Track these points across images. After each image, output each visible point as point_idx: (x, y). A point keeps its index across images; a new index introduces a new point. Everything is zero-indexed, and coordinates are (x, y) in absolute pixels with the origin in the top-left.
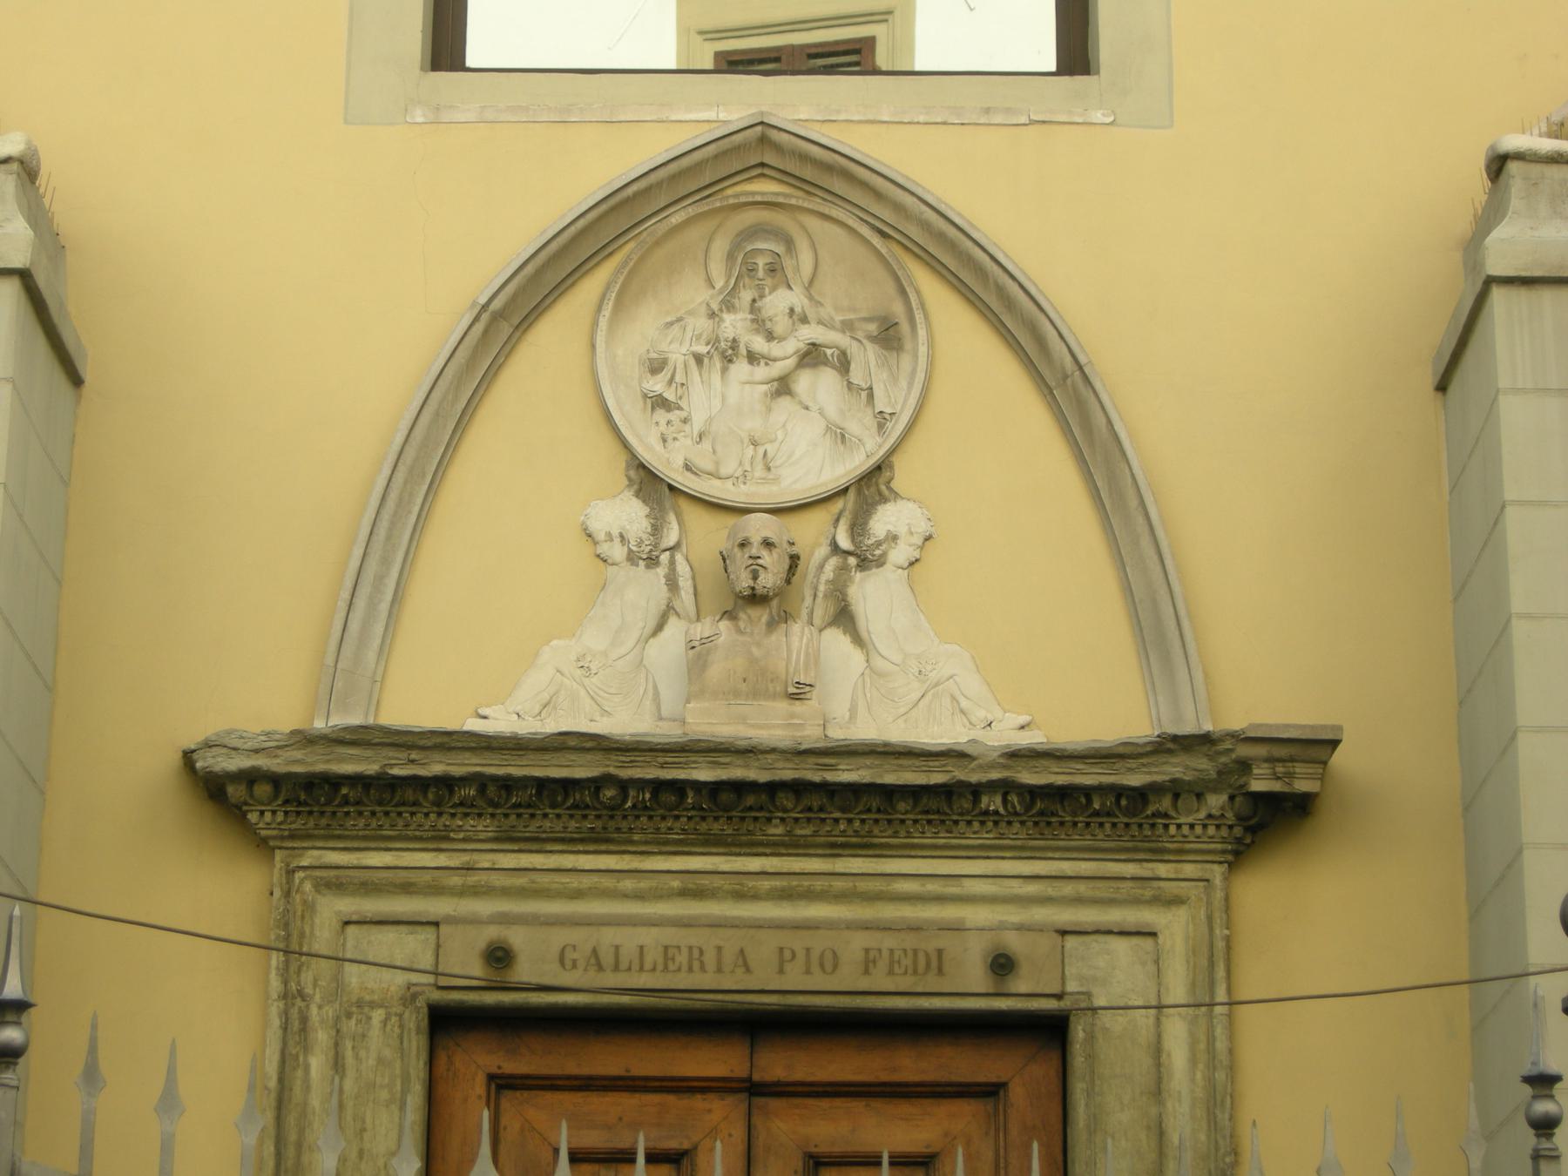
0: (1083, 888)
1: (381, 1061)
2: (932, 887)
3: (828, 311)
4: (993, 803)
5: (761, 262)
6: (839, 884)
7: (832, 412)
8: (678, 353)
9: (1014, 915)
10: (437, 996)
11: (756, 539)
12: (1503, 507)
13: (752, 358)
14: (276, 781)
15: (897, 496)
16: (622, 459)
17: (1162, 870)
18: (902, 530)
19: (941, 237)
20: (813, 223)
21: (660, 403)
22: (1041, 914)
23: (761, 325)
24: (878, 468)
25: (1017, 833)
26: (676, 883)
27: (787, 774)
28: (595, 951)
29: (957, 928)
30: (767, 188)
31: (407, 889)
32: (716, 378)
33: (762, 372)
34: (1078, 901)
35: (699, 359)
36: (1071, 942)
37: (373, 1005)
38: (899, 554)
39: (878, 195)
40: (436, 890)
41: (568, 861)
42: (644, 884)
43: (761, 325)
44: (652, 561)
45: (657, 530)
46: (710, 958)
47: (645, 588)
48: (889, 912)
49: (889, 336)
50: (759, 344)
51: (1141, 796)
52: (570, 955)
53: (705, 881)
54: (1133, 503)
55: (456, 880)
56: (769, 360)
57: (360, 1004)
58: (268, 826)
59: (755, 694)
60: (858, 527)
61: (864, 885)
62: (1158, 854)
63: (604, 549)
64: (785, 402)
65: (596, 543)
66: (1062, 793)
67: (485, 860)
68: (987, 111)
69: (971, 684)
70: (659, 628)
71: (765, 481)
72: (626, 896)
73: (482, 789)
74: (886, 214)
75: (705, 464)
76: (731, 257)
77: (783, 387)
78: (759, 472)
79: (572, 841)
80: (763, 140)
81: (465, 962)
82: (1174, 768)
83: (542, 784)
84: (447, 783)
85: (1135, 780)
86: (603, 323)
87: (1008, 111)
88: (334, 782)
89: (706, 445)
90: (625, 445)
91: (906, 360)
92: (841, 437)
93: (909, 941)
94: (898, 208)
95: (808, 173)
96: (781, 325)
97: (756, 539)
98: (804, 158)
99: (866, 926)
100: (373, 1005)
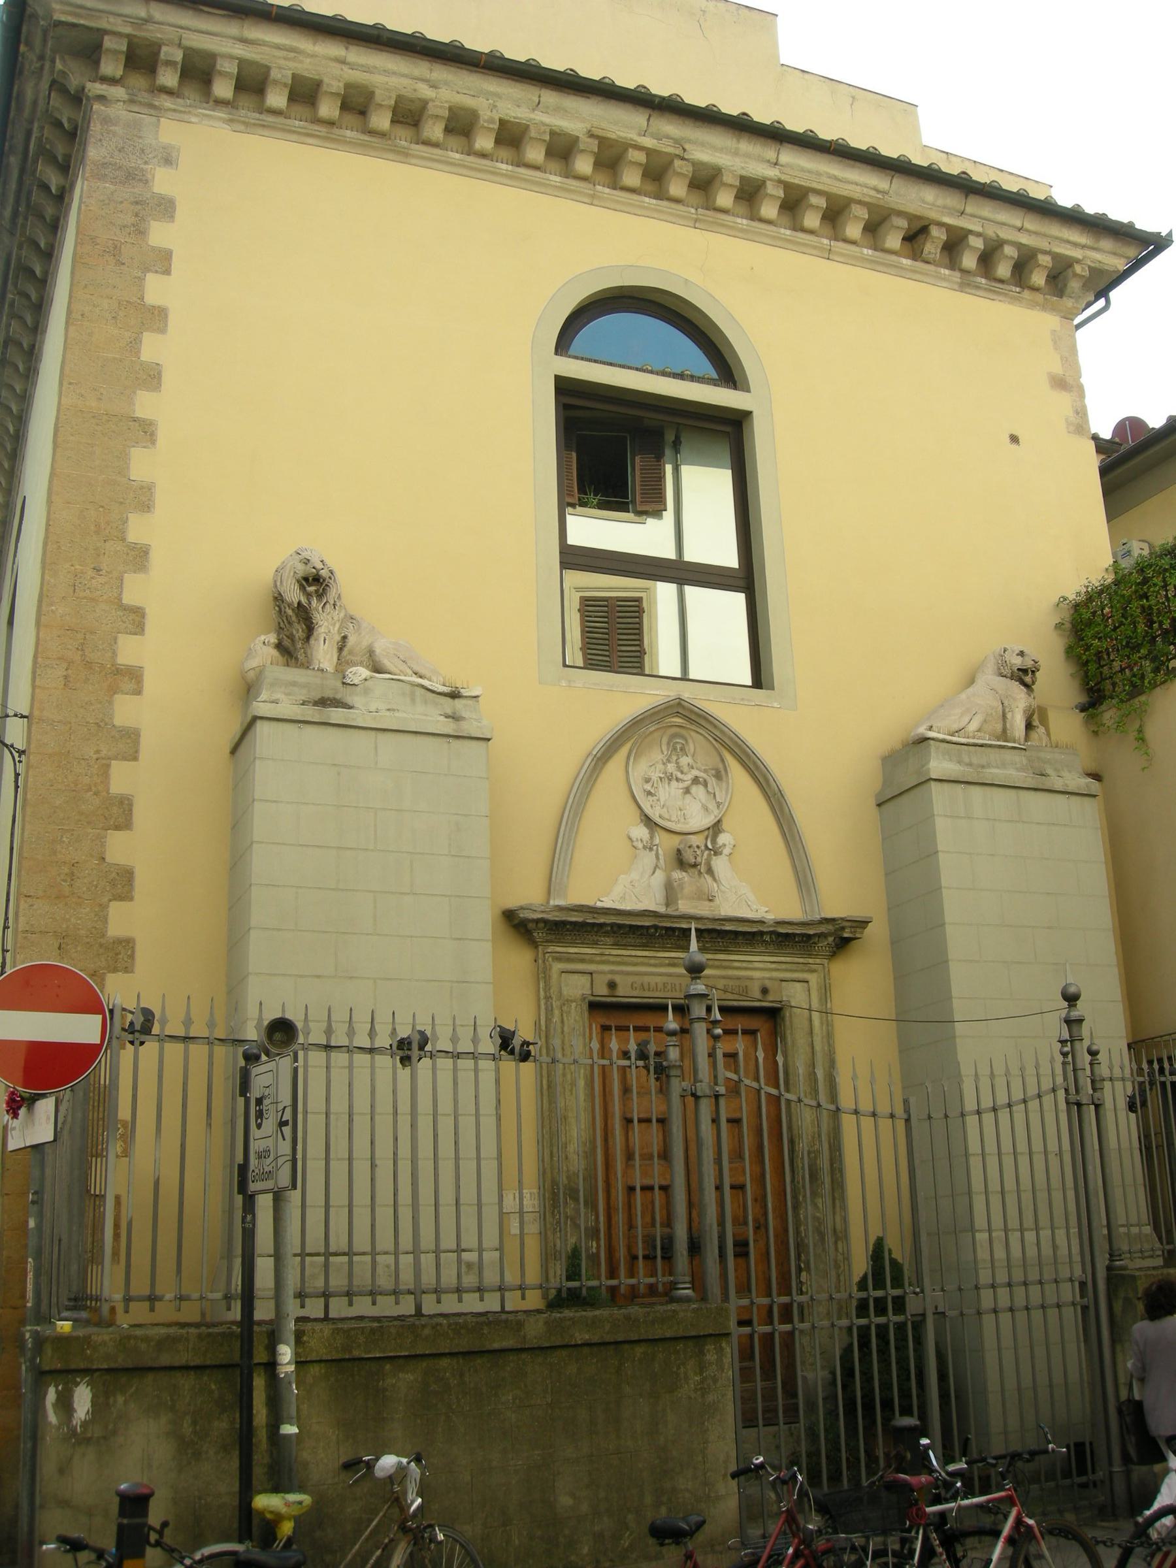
0: (788, 966)
1: (575, 1020)
2: (744, 965)
3: (699, 765)
4: (767, 938)
5: (678, 747)
6: (717, 963)
7: (703, 801)
8: (655, 776)
9: (767, 974)
10: (592, 998)
11: (695, 845)
12: (252, 843)
13: (677, 780)
14: (545, 921)
15: (724, 831)
16: (638, 812)
17: (811, 961)
18: (727, 843)
19: (736, 743)
20: (693, 734)
21: (649, 793)
22: (775, 974)
23: (679, 769)
24: (719, 821)
25: (771, 948)
26: (667, 961)
27: (710, 926)
28: (642, 985)
29: (751, 979)
30: (678, 720)
31: (582, 961)
32: (667, 786)
33: (681, 785)
34: (786, 970)
35: (661, 778)
36: (784, 984)
37: (572, 1001)
38: (726, 851)
39: (715, 726)
40: (592, 962)
41: (634, 953)
42: (657, 962)
43: (679, 769)
44: (651, 849)
45: (652, 838)
46: (678, 988)
47: (648, 859)
48: (730, 973)
49: (718, 776)
50: (679, 775)
51: (809, 937)
52: (635, 985)
53: (676, 961)
54: (798, 838)
55: (598, 958)
56: (683, 781)
57: (567, 1000)
58: (540, 938)
59: (699, 898)
60: (714, 841)
61: (724, 964)
62: (810, 956)
63: (635, 844)
64: (688, 795)
65: (632, 841)
66: (787, 936)
67: (607, 952)
68: (743, 699)
69: (752, 897)
70: (654, 873)
71: (684, 823)
72: (651, 965)
73: (612, 927)
74: (718, 733)
75: (666, 816)
76: (668, 744)
77: (687, 791)
78: (682, 820)
79: (636, 946)
80: (679, 704)
81: (602, 990)
82: (823, 929)
83: (631, 926)
84: (602, 925)
85: (811, 932)
86: (631, 763)
87: (748, 700)
88: (564, 923)
89: (665, 810)
90: (640, 807)
91: (724, 785)
92: (706, 809)
93: (737, 983)
94: (722, 732)
95: (693, 717)
96: (686, 769)
97: (695, 845)
98: (692, 711)
99: (724, 977)
100: (572, 1001)
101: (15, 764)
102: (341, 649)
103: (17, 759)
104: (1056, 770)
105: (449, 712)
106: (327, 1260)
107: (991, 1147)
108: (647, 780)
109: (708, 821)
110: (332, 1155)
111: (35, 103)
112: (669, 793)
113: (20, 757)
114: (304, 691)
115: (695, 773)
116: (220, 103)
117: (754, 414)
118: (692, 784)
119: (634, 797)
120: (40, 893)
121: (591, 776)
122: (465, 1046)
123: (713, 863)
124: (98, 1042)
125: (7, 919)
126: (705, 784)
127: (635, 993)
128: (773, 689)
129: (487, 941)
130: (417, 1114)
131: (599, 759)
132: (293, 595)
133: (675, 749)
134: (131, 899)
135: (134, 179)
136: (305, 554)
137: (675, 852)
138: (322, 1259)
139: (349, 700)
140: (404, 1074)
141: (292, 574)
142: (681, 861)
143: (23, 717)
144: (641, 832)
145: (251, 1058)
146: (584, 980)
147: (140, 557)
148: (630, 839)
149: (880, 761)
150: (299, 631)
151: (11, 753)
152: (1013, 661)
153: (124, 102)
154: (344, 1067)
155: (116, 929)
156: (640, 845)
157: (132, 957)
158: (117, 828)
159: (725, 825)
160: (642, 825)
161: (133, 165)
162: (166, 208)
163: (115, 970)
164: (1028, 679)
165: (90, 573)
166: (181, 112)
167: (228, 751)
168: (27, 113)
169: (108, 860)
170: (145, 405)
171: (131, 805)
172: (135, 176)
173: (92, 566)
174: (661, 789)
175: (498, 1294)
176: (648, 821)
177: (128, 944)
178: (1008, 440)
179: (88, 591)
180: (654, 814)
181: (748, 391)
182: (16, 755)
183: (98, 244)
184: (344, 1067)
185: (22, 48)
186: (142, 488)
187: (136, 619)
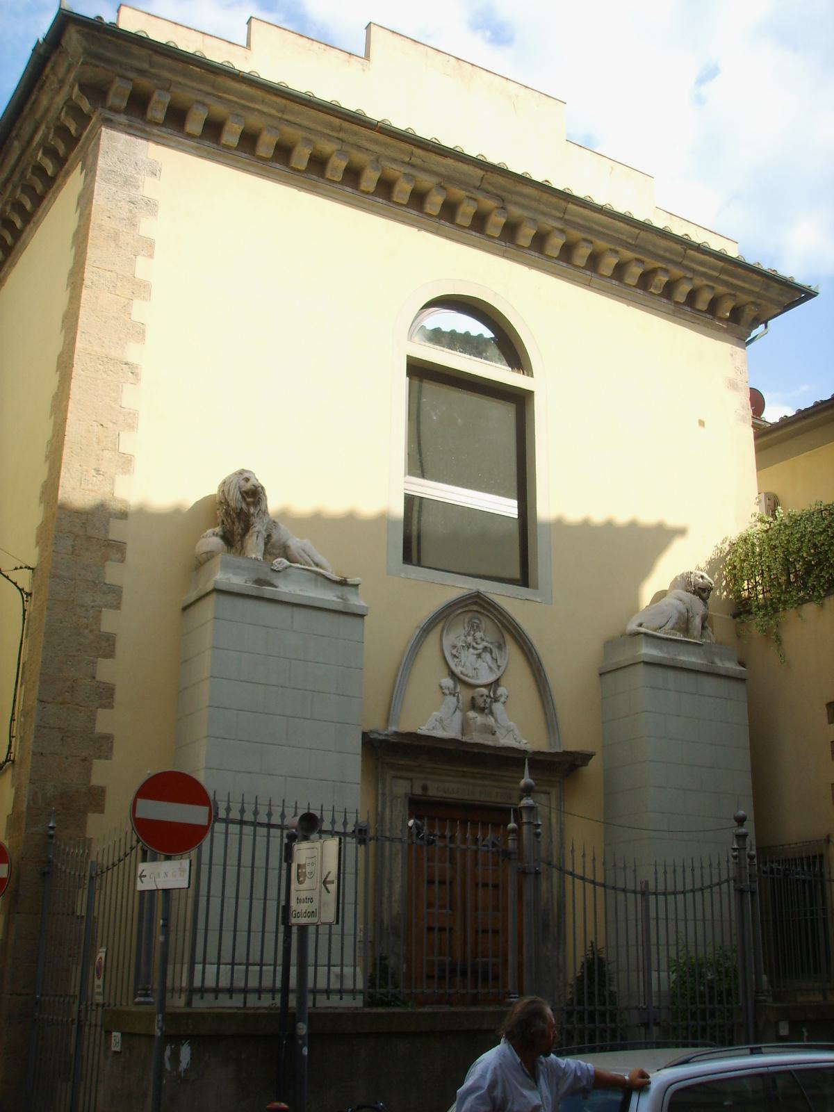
3: (488, 639)
13: (474, 648)
21: (455, 656)
30: (475, 608)
33: (476, 652)
37: (399, 797)
38: (503, 699)
43: (475, 639)
44: (454, 695)
45: (455, 687)
50: (475, 646)
60: (495, 693)
64: (479, 659)
70: (455, 712)
75: (465, 672)
76: (469, 622)
77: (479, 656)
81: (418, 791)
96: (479, 641)
101: (24, 603)
102: (266, 544)
103: (25, 599)
106: (247, 968)
108: (454, 647)
109: (492, 678)
110: (254, 896)
111: (47, 110)
112: (468, 657)
113: (27, 597)
115: (485, 644)
116: (190, 136)
117: (535, 393)
118: (483, 651)
119: (444, 658)
121: (418, 643)
122: (263, 818)
123: (493, 707)
124: (207, 824)
125: (13, 714)
126: (491, 652)
129: (358, 754)
130: (287, 870)
131: (425, 630)
134: (112, 707)
135: (130, 184)
136: (246, 475)
137: (470, 698)
138: (244, 967)
139: (276, 582)
140: (362, 848)
141: (237, 489)
142: (473, 705)
143: (29, 568)
144: (448, 682)
145: (292, 838)
146: (407, 784)
148: (441, 687)
150: (238, 528)
151: (22, 596)
153: (125, 125)
154: (264, 836)
155: (101, 728)
156: (447, 692)
157: (111, 748)
158: (105, 656)
159: (503, 682)
161: (129, 174)
162: (151, 206)
163: (99, 757)
164: (704, 595)
165: (93, 472)
166: (164, 138)
167: (181, 607)
168: (38, 116)
169: (98, 678)
170: (133, 353)
171: (114, 641)
172: (128, 182)
174: (462, 655)
176: (452, 674)
177: (108, 738)
178: (698, 423)
179: (90, 486)
180: (457, 670)
181: (532, 376)
182: (25, 596)
183: (103, 231)
184: (264, 836)
185: (48, 70)
186: (130, 413)
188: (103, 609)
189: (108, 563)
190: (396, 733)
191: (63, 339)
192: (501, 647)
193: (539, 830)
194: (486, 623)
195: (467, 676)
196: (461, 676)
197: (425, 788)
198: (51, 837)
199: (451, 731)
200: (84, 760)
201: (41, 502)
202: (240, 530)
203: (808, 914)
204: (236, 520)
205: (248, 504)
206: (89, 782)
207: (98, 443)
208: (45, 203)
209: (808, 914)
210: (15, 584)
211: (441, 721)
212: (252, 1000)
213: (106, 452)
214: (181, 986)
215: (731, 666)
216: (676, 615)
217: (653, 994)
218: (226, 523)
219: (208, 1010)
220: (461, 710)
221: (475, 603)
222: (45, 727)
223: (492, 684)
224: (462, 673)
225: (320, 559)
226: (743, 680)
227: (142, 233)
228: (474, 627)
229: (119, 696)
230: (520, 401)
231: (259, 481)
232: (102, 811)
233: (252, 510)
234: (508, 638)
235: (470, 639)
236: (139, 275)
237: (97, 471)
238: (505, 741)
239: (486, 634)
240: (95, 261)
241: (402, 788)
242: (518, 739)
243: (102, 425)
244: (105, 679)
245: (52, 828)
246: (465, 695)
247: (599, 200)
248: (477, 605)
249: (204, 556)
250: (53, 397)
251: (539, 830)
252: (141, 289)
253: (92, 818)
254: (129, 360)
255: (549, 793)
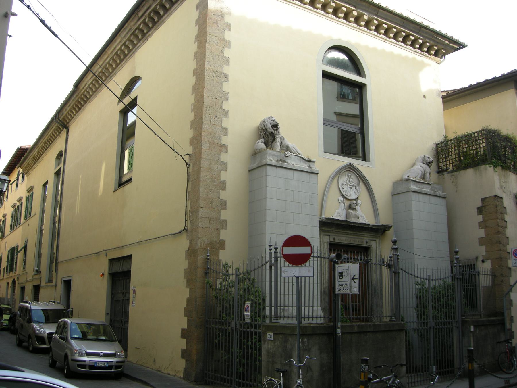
13: (349, 185)
33: (350, 187)
38: (359, 205)
45: (343, 200)
50: (350, 184)
75: (347, 194)
81: (332, 240)
96: (351, 182)
104: (437, 190)
105: (308, 165)
107: (286, 293)
108: (343, 185)
114: (277, 157)
117: (367, 85)
120: (204, 207)
124: (310, 253)
126: (355, 187)
127: (339, 241)
128: (370, 162)
132: (270, 129)
133: (349, 177)
144: (341, 198)
146: (328, 237)
147: (226, 113)
148: (339, 200)
149: (392, 183)
150: (270, 139)
152: (427, 160)
155: (222, 217)
156: (341, 202)
157: (226, 225)
158: (223, 190)
159: (359, 198)
160: (341, 197)
163: (222, 229)
164: (430, 165)
165: (214, 117)
171: (225, 183)
173: (215, 115)
175: (316, 319)
178: (423, 97)
180: (344, 194)
181: (366, 78)
186: (226, 93)
187: (225, 131)
188: (221, 171)
189: (222, 153)
190: (326, 218)
191: (196, 63)
192: (359, 184)
193: (399, 257)
194: (353, 176)
195: (347, 196)
196: (345, 196)
197: (334, 239)
198: (208, 259)
199: (342, 218)
200: (217, 230)
201: (191, 129)
202: (271, 140)
203: (465, 286)
204: (270, 136)
205: (274, 130)
206: (219, 238)
207: (215, 106)
208: (176, 6)
209: (465, 286)
210: (185, 161)
211: (339, 213)
212: (311, 321)
213: (218, 109)
214: (299, 317)
215: (440, 193)
216: (421, 173)
217: (272, 316)
218: (265, 137)
219: (308, 325)
220: (346, 209)
221: (350, 168)
222: (203, 217)
223: (355, 199)
224: (346, 195)
225: (300, 152)
226: (445, 198)
227: (226, 21)
228: (349, 177)
229: (228, 204)
230: (361, 87)
231: (276, 120)
232: (224, 249)
233: (276, 132)
234: (361, 181)
235: (348, 182)
236: (226, 38)
237: (216, 116)
238: (362, 221)
239: (354, 179)
240: (210, 32)
241: (326, 239)
242: (365, 220)
243: (216, 98)
244: (223, 199)
245: (208, 256)
246: (347, 203)
247: (391, 8)
248: (351, 168)
249: (258, 151)
250: (193, 86)
251: (399, 257)
252: (227, 43)
253: (221, 252)
254: (225, 72)
255: (376, 241)
